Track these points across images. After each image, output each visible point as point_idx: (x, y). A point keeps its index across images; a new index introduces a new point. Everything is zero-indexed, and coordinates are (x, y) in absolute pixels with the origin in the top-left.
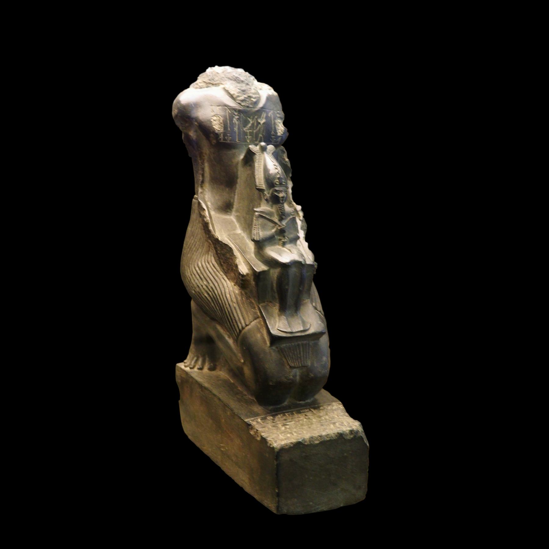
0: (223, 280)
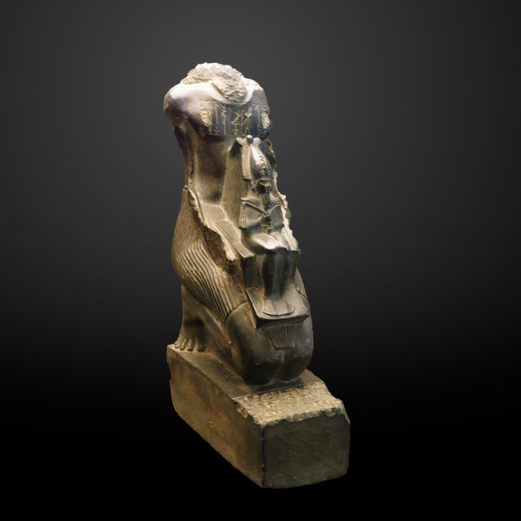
0: (211, 266)
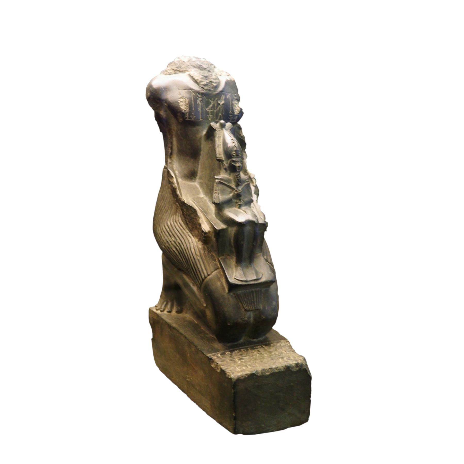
0: (188, 237)
